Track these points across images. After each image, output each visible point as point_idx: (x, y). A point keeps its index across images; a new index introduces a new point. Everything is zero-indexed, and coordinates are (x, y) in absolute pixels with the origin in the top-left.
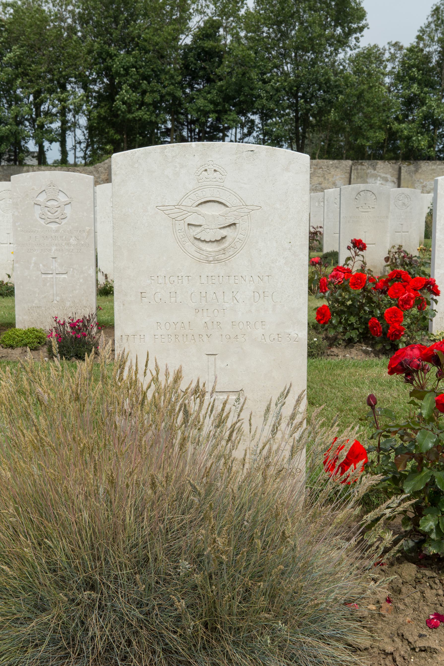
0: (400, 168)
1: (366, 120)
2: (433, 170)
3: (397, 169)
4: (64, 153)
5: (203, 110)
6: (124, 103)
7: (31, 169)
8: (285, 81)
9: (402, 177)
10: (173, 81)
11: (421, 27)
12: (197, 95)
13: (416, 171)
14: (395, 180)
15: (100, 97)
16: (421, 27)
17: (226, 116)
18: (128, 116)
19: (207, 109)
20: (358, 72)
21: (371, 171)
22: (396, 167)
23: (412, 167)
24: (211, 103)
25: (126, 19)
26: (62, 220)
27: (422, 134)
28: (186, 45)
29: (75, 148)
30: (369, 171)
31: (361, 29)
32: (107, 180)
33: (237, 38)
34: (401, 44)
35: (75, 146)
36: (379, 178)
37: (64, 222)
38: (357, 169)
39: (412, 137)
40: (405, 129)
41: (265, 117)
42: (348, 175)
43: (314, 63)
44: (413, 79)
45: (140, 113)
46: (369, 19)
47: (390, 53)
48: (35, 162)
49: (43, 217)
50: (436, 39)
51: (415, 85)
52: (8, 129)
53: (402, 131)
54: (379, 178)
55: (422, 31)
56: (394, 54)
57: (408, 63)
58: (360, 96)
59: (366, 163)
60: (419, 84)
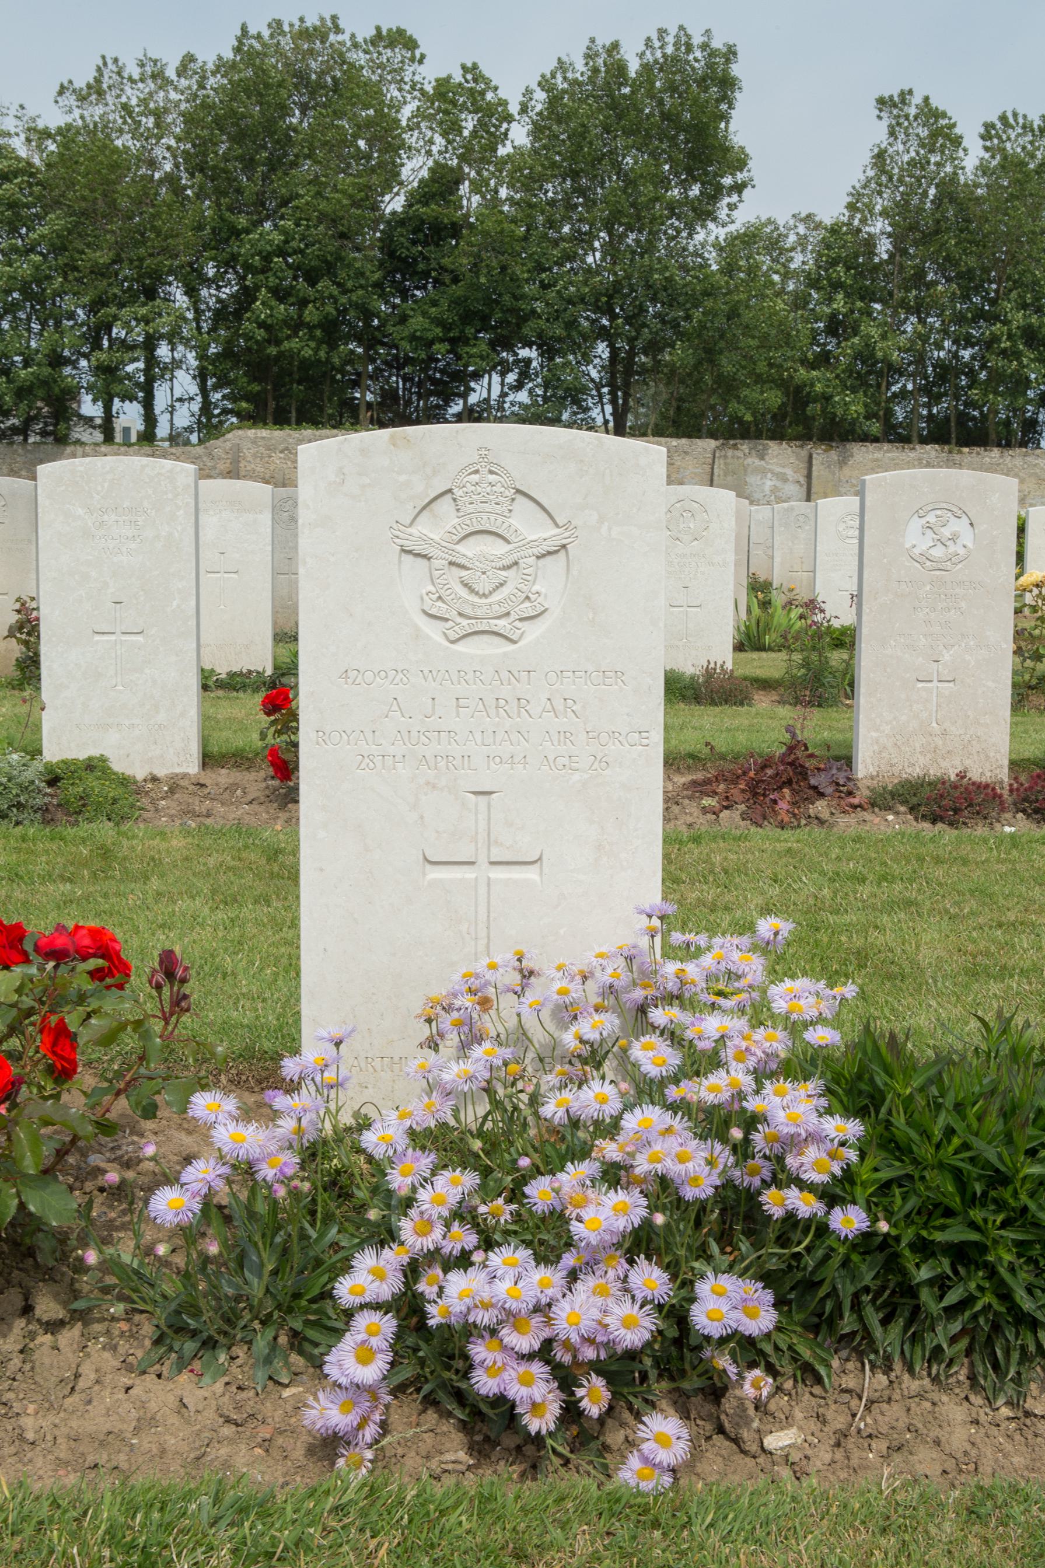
0: (810, 457)
1: (744, 363)
2: (877, 460)
3: (806, 459)
4: (150, 419)
5: (420, 338)
6: (262, 325)
7: (79, 450)
8: (585, 283)
9: (815, 474)
10: (363, 282)
11: (854, 188)
12: (412, 309)
13: (843, 463)
14: (803, 480)
15: (221, 315)
16: (854, 188)
17: (467, 349)
18: (268, 351)
19: (430, 335)
20: (729, 269)
21: (753, 461)
22: (804, 453)
23: (834, 455)
24: (437, 326)
25: (248, 180)
26: (524, 626)
27: (854, 391)
28: (394, 213)
29: (171, 409)
30: (749, 461)
31: (739, 188)
32: (229, 472)
33: (495, 203)
34: (817, 219)
35: (172, 406)
36: (769, 475)
37: (533, 632)
38: (725, 457)
39: (831, 397)
40: (818, 380)
41: (548, 351)
42: (708, 468)
43: (649, 248)
44: (837, 285)
45: (294, 344)
46: (755, 168)
47: (798, 234)
48: (99, 436)
49: (439, 609)
50: (878, 208)
51: (840, 296)
52: (32, 373)
53: (812, 385)
54: (769, 475)
55: (857, 195)
56: (806, 237)
57: (828, 256)
58: (733, 314)
59: (745, 446)
60: (847, 295)
